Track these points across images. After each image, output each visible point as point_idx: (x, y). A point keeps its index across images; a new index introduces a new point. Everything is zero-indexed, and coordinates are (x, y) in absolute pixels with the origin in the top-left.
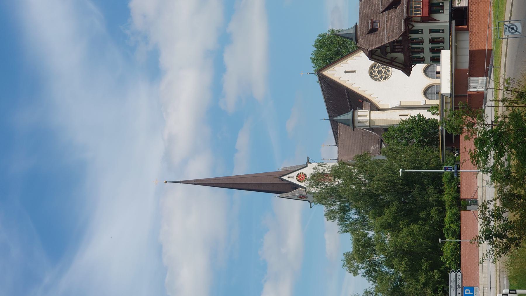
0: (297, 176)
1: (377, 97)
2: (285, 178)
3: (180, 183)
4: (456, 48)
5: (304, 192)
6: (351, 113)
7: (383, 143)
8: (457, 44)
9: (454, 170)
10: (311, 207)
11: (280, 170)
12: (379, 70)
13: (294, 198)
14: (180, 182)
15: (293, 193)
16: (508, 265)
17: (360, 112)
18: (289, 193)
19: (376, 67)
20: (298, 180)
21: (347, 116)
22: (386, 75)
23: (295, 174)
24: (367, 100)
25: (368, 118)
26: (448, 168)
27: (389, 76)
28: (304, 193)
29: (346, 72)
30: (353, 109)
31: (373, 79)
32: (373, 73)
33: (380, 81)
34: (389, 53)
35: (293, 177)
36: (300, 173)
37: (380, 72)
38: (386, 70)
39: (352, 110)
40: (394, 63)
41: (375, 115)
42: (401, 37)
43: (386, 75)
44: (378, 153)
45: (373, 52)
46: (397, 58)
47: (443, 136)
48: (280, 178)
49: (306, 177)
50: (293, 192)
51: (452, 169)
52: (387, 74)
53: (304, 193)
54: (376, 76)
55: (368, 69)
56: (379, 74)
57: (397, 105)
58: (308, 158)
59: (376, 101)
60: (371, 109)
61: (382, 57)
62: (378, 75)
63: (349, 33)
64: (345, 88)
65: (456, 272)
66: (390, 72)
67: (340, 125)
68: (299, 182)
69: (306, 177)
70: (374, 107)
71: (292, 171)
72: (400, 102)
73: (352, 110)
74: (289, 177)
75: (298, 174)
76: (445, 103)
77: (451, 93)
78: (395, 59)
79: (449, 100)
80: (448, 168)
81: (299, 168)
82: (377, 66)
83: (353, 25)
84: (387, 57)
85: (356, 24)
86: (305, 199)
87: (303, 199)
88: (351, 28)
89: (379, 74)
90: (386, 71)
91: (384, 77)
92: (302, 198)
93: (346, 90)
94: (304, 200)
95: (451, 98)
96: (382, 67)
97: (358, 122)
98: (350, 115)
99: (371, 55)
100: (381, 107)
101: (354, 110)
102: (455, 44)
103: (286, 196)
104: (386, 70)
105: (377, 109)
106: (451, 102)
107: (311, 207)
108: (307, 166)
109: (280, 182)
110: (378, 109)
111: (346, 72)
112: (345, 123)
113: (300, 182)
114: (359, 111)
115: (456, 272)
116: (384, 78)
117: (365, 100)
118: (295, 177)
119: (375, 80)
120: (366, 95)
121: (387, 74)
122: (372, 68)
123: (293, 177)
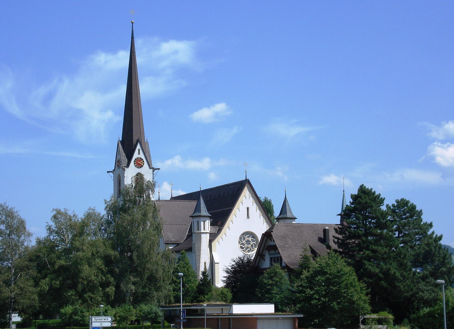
0: (140, 158)
1: (223, 240)
2: (138, 147)
3: (132, 38)
4: (277, 319)
5: (124, 166)
6: (207, 214)
7: (176, 246)
8: (281, 319)
9: (182, 319)
10: (108, 172)
11: (146, 141)
12: (250, 241)
13: (118, 155)
14: (132, 38)
15: (123, 154)
16: (400, 326)
17: (208, 223)
18: (123, 151)
19: (253, 239)
20: (136, 159)
21: (204, 211)
22: (245, 249)
23: (142, 156)
24: (219, 231)
25: (202, 231)
26: (184, 314)
27: (244, 252)
28: (123, 166)
29: (248, 209)
30: (211, 216)
31: (241, 236)
32: (247, 236)
33: (239, 242)
34: (269, 253)
35: (139, 154)
36: (143, 162)
37: (248, 242)
38: (250, 249)
39: (210, 215)
40: (259, 257)
41: (205, 239)
42: (285, 265)
43: (245, 249)
44: (165, 241)
45: (270, 237)
46: (264, 261)
47: (191, 307)
48: (138, 141)
49: (139, 167)
50: (124, 154)
51: (184, 317)
52: (246, 249)
53: (123, 166)
54: (244, 239)
55: (251, 231)
56: (246, 241)
57: (216, 260)
58: (159, 169)
59: (218, 238)
60: (211, 234)
61: (264, 247)
62: (245, 241)
63: (287, 211)
64: (232, 208)
65: (111, 321)
66: (248, 253)
67: (194, 203)
68: (134, 160)
69: (139, 167)
70: (213, 237)
71: (145, 153)
72: (218, 263)
73: (210, 215)
74: (139, 150)
75: (142, 159)
76: (222, 309)
77: (233, 314)
78: (262, 258)
79: (225, 312)
80: (184, 314)
81: (148, 160)
82: (254, 240)
83: (295, 215)
84: (264, 250)
85: (294, 218)
86: (117, 166)
87: (116, 164)
88: (291, 213)
89: (246, 241)
90: (249, 249)
91: (243, 247)
92: (118, 163)
93: (229, 208)
94: (116, 165)
95: (228, 314)
96: (253, 245)
97: (198, 222)
98: (205, 213)
99: (267, 235)
100: (213, 244)
101: (210, 218)
102: (281, 317)
103: (120, 147)
104: (250, 249)
105: (212, 239)
106: (223, 314)
107: (108, 172)
108: (150, 168)
109: (134, 142)
110: (211, 241)
111: (248, 209)
112: (198, 209)
113: (135, 161)
114: (209, 221)
115: (111, 321)
116: (242, 246)
117: (220, 228)
118: (139, 156)
119: (240, 238)
120: (225, 229)
121: (246, 249)
122: (253, 235)
123: (139, 154)
